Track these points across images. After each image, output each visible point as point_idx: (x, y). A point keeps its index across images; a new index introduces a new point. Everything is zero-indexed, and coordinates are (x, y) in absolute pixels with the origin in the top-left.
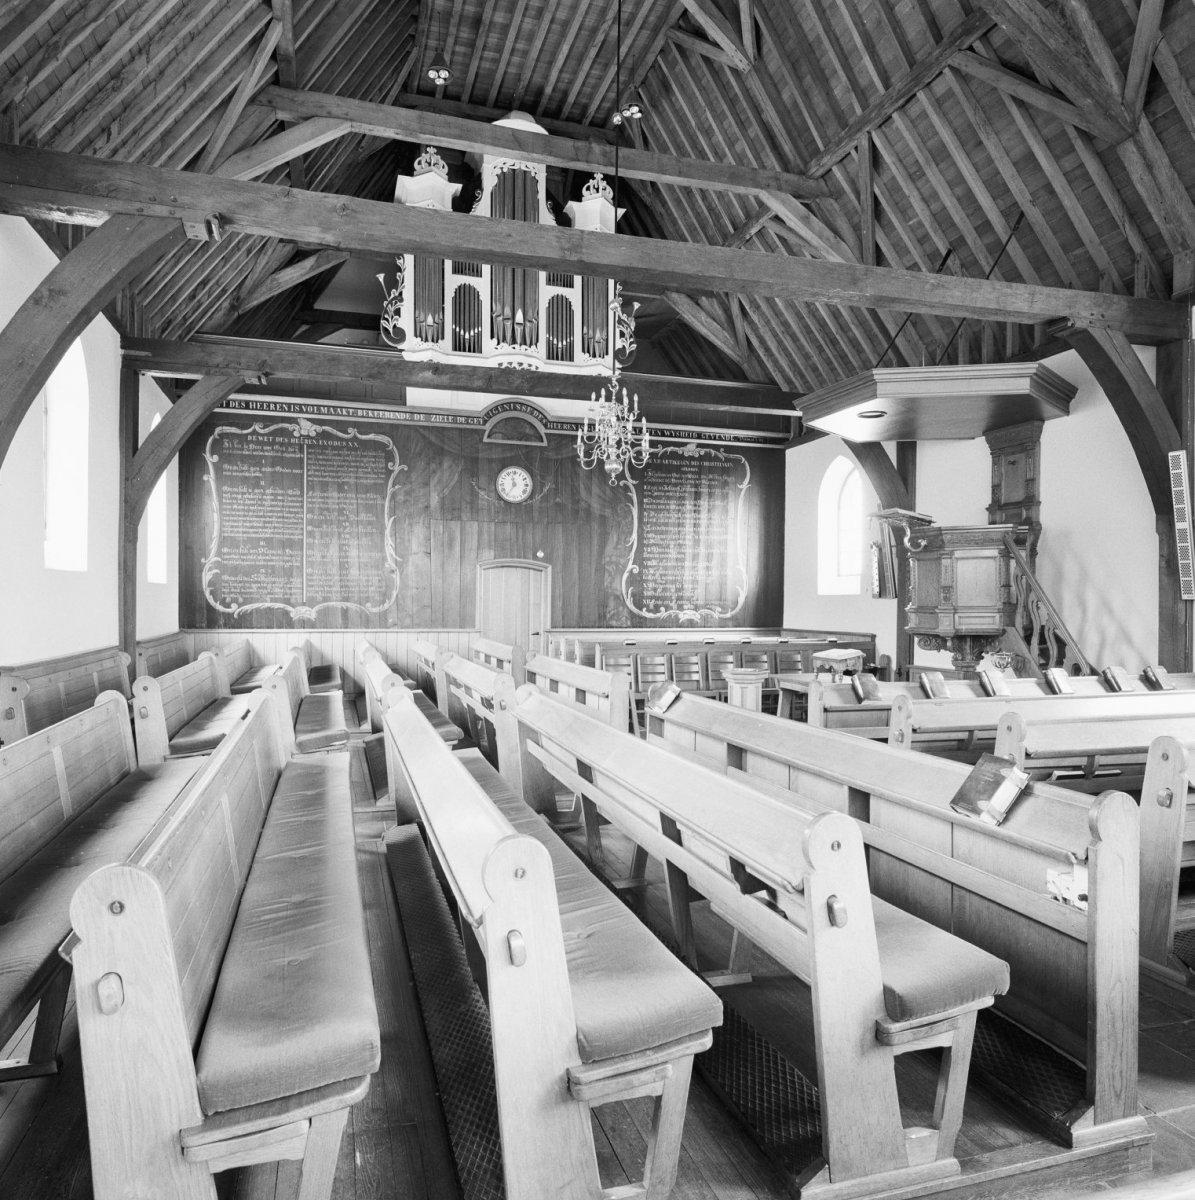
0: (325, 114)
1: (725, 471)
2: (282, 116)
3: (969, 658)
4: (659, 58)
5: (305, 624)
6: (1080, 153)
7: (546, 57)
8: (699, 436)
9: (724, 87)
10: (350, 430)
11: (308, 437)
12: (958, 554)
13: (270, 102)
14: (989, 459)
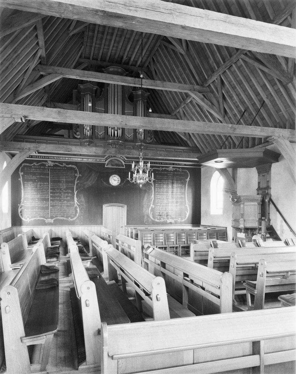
0: (55, 72)
1: (181, 175)
2: (42, 73)
3: (250, 235)
4: (159, 48)
5: (50, 224)
6: (278, 85)
7: (123, 48)
8: (173, 164)
9: (178, 58)
10: (64, 164)
11: (50, 166)
12: (246, 204)
13: (38, 70)
14: (257, 174)
